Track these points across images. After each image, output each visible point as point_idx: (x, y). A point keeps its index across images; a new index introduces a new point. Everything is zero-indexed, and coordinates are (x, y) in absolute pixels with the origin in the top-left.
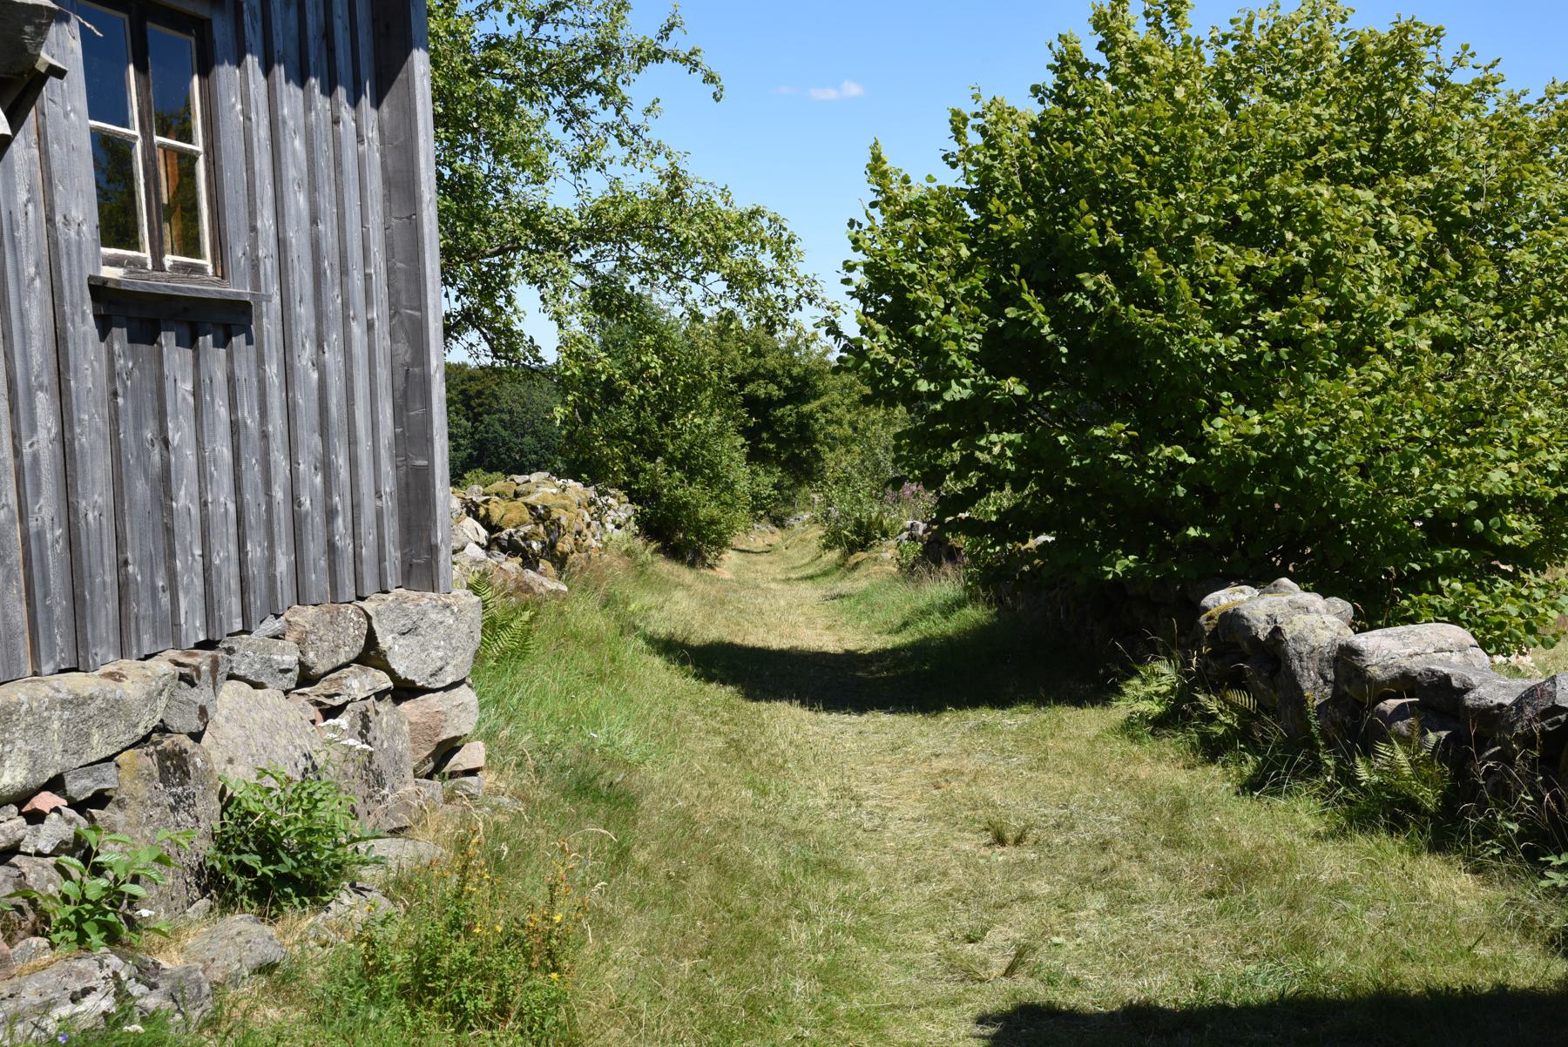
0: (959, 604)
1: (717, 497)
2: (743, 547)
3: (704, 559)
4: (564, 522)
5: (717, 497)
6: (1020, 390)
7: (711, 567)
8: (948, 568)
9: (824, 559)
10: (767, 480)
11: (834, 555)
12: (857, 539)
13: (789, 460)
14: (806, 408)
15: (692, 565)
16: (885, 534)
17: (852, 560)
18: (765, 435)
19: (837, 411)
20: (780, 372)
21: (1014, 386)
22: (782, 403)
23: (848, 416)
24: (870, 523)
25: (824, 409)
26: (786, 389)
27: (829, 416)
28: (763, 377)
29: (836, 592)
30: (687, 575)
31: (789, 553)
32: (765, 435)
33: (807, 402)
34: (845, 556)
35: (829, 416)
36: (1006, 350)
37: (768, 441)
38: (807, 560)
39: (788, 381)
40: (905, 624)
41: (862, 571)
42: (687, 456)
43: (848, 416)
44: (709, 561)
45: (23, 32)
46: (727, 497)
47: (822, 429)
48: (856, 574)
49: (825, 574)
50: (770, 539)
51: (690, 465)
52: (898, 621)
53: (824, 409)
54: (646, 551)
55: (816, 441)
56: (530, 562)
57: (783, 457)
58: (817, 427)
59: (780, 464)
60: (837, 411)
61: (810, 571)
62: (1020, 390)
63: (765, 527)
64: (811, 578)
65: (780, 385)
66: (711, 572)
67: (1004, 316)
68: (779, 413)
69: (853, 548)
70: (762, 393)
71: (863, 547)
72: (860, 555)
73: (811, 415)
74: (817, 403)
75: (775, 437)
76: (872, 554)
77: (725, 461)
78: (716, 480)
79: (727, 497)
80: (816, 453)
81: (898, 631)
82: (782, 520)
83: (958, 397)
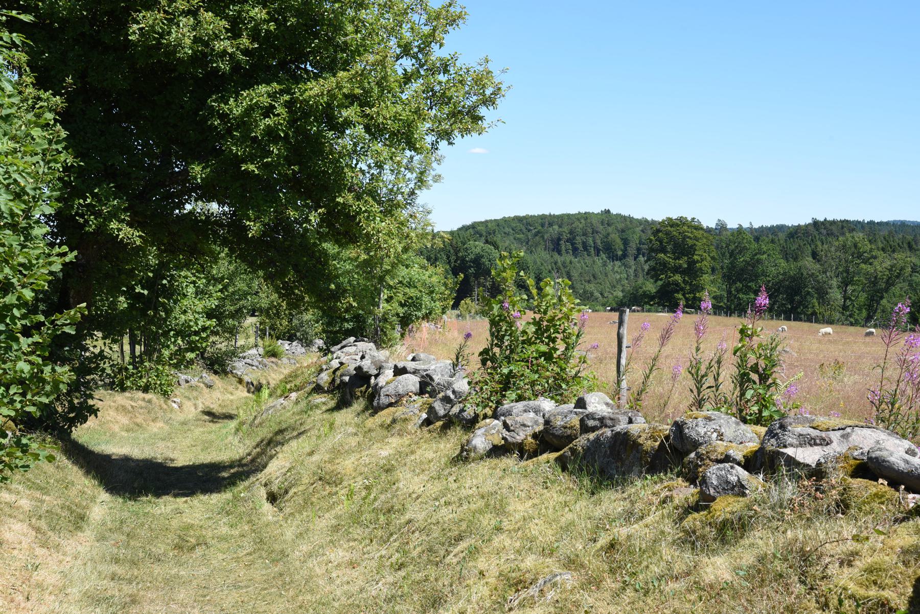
22: (245, 77)
63: (197, 375)
68: (235, 108)
82: (223, 365)
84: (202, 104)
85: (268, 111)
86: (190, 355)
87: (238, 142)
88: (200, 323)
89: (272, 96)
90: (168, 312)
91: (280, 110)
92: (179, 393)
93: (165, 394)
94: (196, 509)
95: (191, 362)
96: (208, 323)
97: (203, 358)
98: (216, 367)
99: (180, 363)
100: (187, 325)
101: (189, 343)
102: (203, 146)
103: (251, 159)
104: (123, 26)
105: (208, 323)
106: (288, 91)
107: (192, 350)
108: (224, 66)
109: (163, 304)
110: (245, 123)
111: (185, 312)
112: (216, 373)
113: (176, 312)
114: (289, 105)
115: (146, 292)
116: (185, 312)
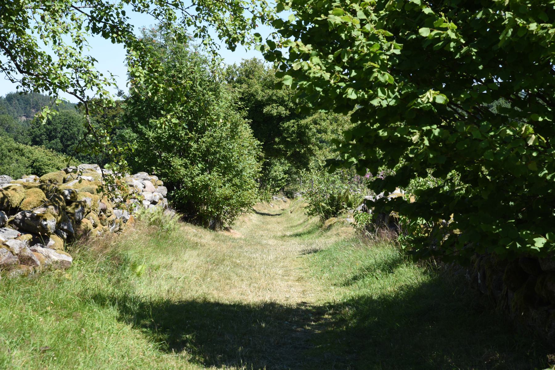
0: (390, 267)
1: (230, 180)
2: (266, 211)
3: (222, 224)
4: (89, 203)
5: (230, 180)
6: (441, 99)
7: (227, 229)
8: (386, 233)
9: (310, 221)
10: (281, 168)
11: (316, 219)
12: (333, 207)
13: (292, 155)
14: (303, 122)
15: (213, 228)
16: (350, 205)
17: (327, 223)
18: (277, 140)
19: (323, 124)
20: (286, 98)
21: (431, 97)
22: (288, 118)
23: (331, 127)
24: (339, 198)
25: (315, 122)
26: (291, 109)
27: (318, 127)
28: (275, 102)
29: (314, 247)
30: (204, 236)
31: (292, 215)
32: (277, 140)
33: (304, 118)
34: (323, 220)
35: (318, 127)
36: (420, 64)
37: (279, 143)
38: (302, 221)
39: (292, 105)
40: (355, 278)
41: (333, 231)
42: (207, 152)
43: (331, 127)
44: (226, 225)
45: (401, 121)
46: (237, 181)
47: (314, 135)
48: (329, 233)
49: (309, 232)
50: (283, 206)
51: (210, 160)
52: (350, 276)
53: (315, 122)
54: (172, 217)
55: (310, 143)
56: (40, 236)
57: (289, 153)
58: (310, 134)
59: (288, 158)
60: (323, 124)
61: (300, 230)
62: (441, 99)
63: (281, 197)
64: (297, 235)
65: (286, 107)
66: (226, 233)
67: (417, 33)
68: (286, 125)
69: (328, 215)
70: (274, 112)
71: (335, 214)
72: (332, 220)
73: (307, 127)
74: (311, 118)
75: (283, 141)
76: (340, 218)
77: (236, 154)
78: (228, 169)
79: (237, 181)
80: (310, 152)
81: (347, 284)
82: (291, 194)
83: (384, 104)
84: (278, 124)
85: (293, 126)
86: (278, 189)
87: (286, 134)
88: (282, 176)
89: (294, 123)
90: (269, 172)
91: (295, 126)
92: (273, 203)
93: (268, 201)
94: (273, 219)
95: (278, 191)
96: (285, 176)
97: (283, 191)
98: (289, 195)
99: (275, 193)
100: (276, 176)
101: (277, 184)
102: (279, 133)
103: (289, 137)
104: (263, 108)
105: (285, 176)
106: (298, 122)
107: (278, 187)
108: (284, 116)
109: (267, 169)
110: (288, 129)
111: (275, 172)
112: (288, 197)
113: (272, 172)
114: (298, 125)
115: (405, 136)
116: (275, 172)
